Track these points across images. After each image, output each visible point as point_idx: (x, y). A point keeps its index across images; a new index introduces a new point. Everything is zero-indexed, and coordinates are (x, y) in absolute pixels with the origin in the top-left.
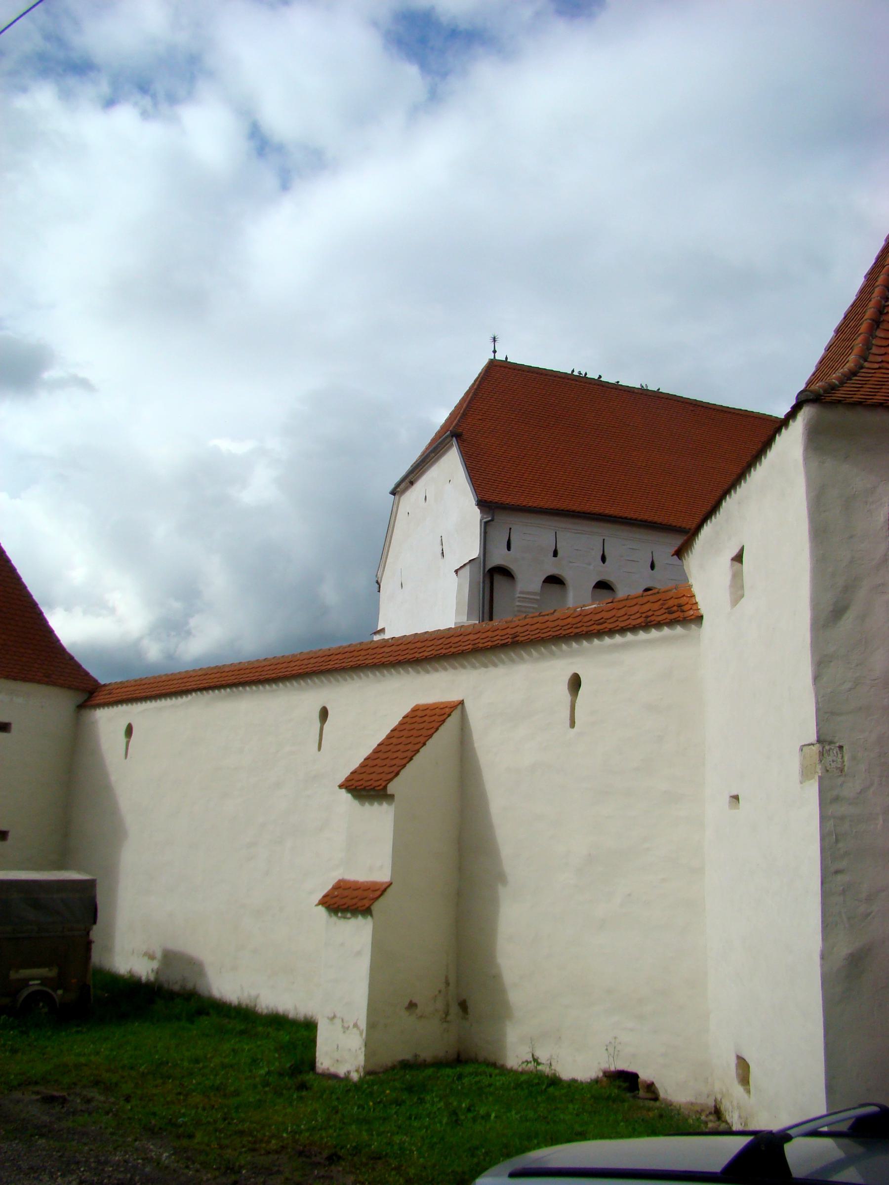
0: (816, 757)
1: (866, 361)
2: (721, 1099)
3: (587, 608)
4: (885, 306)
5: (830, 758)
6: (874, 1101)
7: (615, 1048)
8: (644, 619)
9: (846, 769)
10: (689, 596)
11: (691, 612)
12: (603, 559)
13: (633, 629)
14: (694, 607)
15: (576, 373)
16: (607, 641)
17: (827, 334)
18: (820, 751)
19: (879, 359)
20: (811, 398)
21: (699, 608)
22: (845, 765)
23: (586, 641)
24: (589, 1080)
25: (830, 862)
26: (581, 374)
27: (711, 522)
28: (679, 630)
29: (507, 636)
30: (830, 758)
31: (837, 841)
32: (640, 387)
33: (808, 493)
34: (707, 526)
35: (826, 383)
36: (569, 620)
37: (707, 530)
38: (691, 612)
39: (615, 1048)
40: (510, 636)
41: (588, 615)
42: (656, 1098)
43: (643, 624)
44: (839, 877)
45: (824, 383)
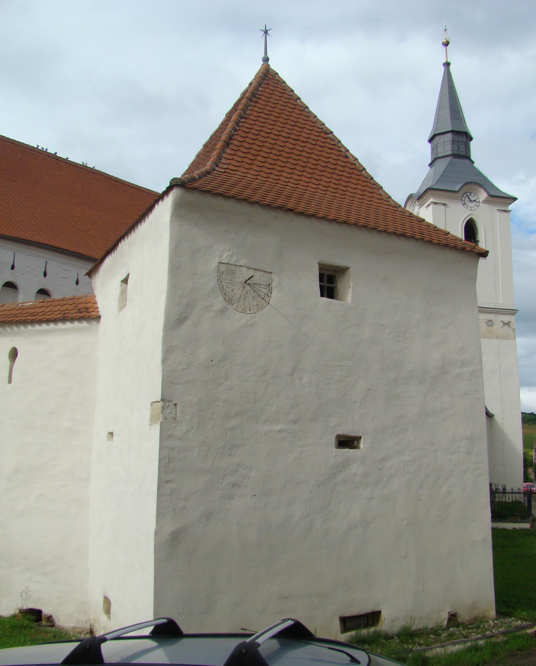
0: (160, 410)
1: (217, 166)
2: (94, 624)
3: (26, 304)
4: (234, 135)
5: (169, 411)
6: (164, 617)
7: (27, 594)
8: (63, 315)
9: (177, 418)
10: (93, 302)
11: (94, 313)
12: (45, 274)
13: (55, 321)
14: (96, 310)
15: (40, 148)
16: (37, 327)
17: (199, 147)
18: (162, 406)
19: (226, 166)
20: (179, 184)
21: (99, 311)
22: (177, 416)
23: (24, 327)
24: (10, 616)
25: (164, 475)
26: (44, 149)
27: (111, 256)
28: (85, 324)
30: (169, 411)
31: (169, 462)
32: (82, 164)
33: (170, 243)
34: (108, 258)
35: (190, 176)
37: (108, 261)
38: (94, 313)
39: (27, 594)
41: (27, 309)
42: (53, 626)
43: (62, 318)
44: (169, 485)
45: (189, 176)
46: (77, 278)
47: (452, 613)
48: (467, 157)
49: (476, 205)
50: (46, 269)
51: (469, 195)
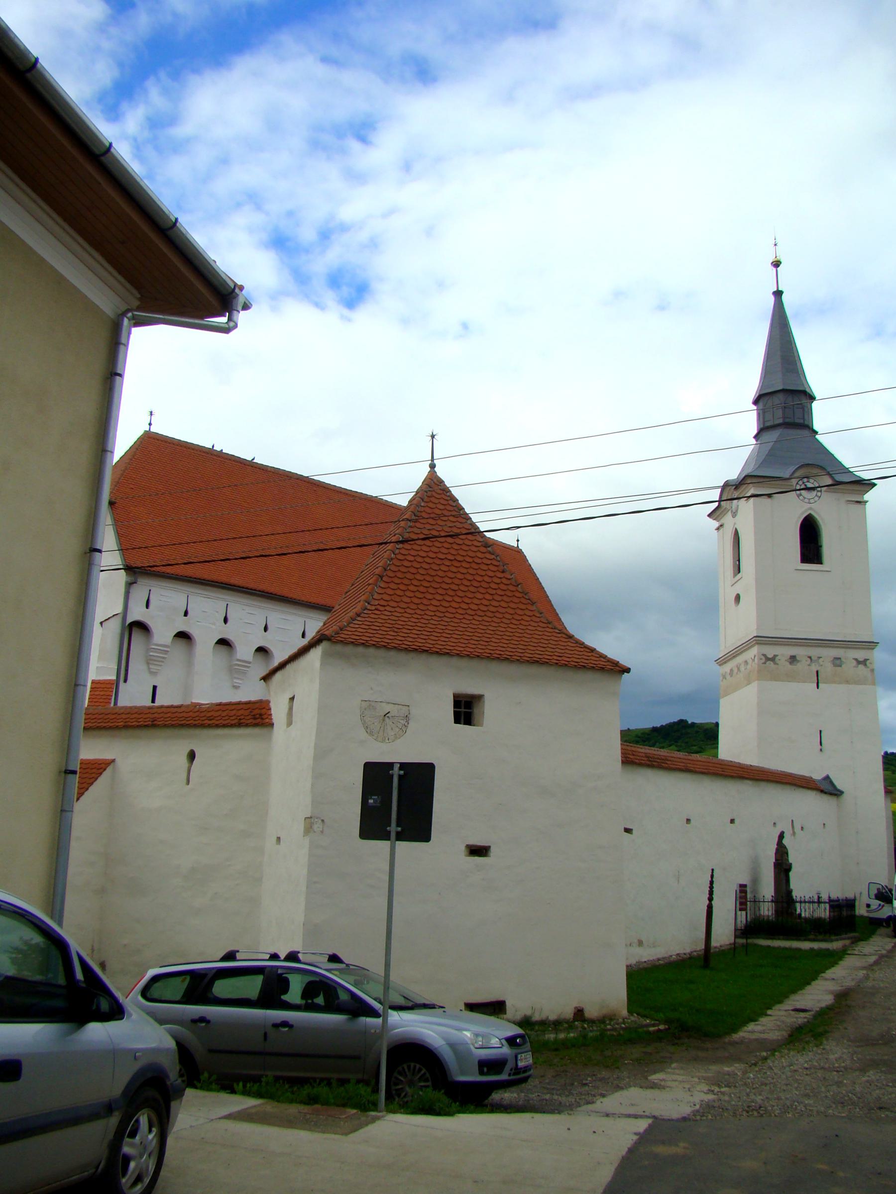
11: (267, 720)
12: (226, 620)
14: (269, 717)
29: (148, 719)
36: (191, 714)
40: (151, 720)
46: (265, 623)
47: (579, 1008)
48: (805, 426)
49: (816, 495)
50: (226, 614)
51: (807, 482)
